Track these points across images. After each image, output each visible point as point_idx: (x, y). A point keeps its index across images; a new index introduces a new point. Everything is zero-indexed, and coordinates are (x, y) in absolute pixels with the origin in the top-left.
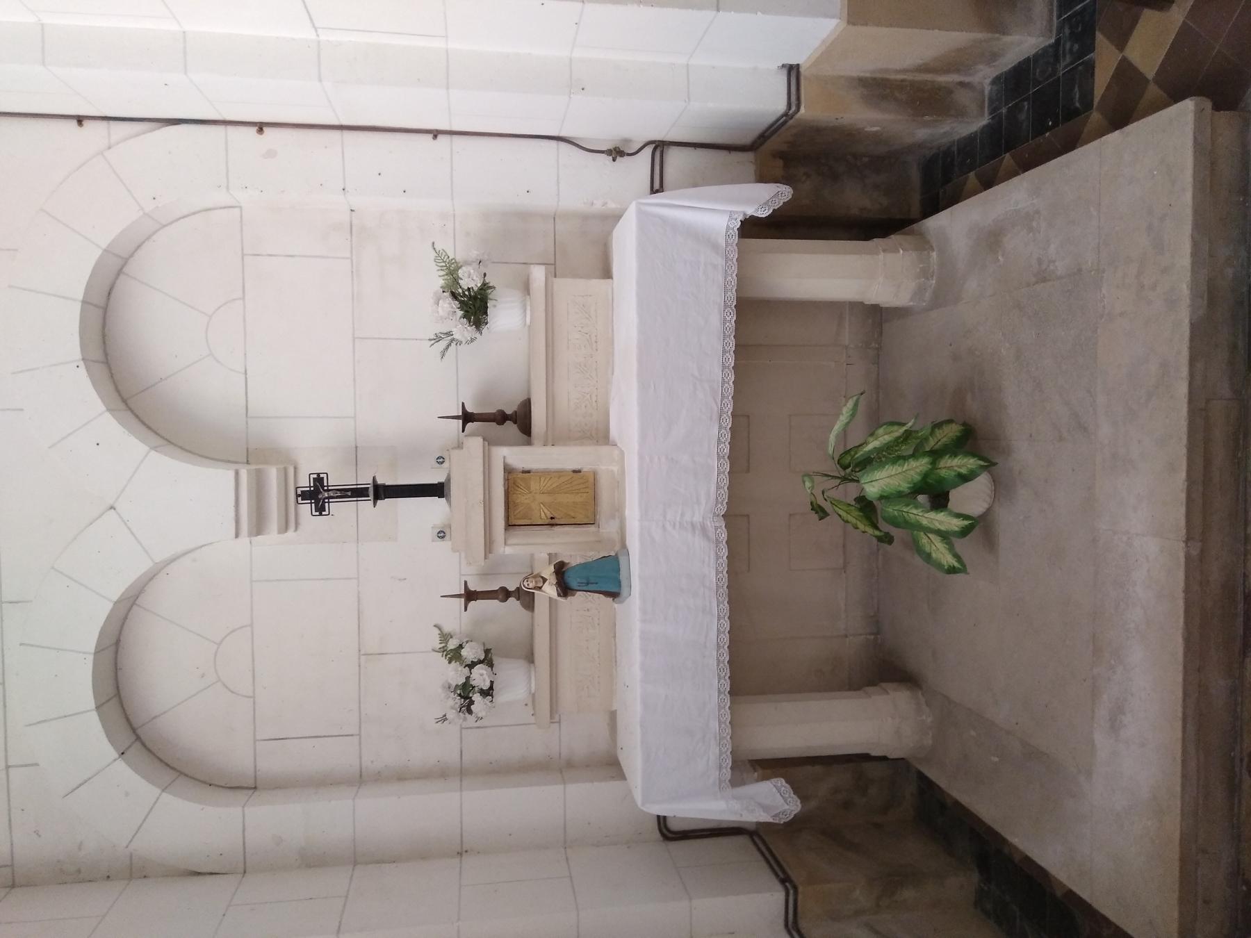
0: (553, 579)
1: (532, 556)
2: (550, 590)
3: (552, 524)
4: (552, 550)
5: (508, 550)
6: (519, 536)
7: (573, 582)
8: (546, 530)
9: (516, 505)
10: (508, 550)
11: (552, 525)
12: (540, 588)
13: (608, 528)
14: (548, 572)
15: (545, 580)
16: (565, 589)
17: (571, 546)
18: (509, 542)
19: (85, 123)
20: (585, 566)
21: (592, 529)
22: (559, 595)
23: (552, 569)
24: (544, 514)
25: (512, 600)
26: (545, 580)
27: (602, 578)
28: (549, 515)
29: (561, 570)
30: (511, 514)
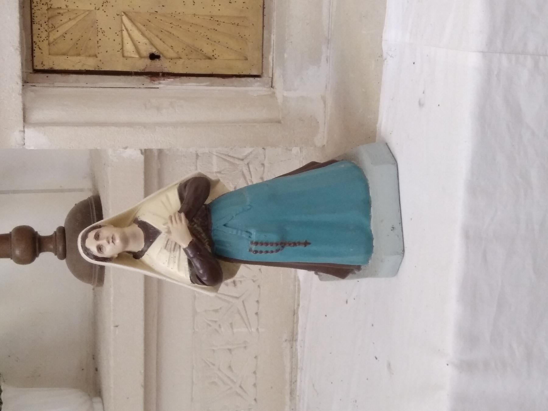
0: (179, 234)
1: (96, 158)
2: (169, 260)
3: (154, 72)
4: (155, 141)
5: (35, 139)
6: (61, 102)
7: (233, 232)
8: (139, 89)
9: (54, 13)
10: (35, 139)
11: (154, 75)
12: (137, 256)
13: (302, 86)
14: (163, 209)
15: (150, 234)
16: (211, 262)
17: (195, 130)
18: (36, 115)
19: (22, 134)
20: (271, 192)
21: (255, 88)
22: (196, 279)
23: (173, 200)
24: (132, 45)
25: (47, 259)
26: (150, 234)
27: (327, 216)
28: (147, 49)
29: (199, 202)
30: (40, 32)
